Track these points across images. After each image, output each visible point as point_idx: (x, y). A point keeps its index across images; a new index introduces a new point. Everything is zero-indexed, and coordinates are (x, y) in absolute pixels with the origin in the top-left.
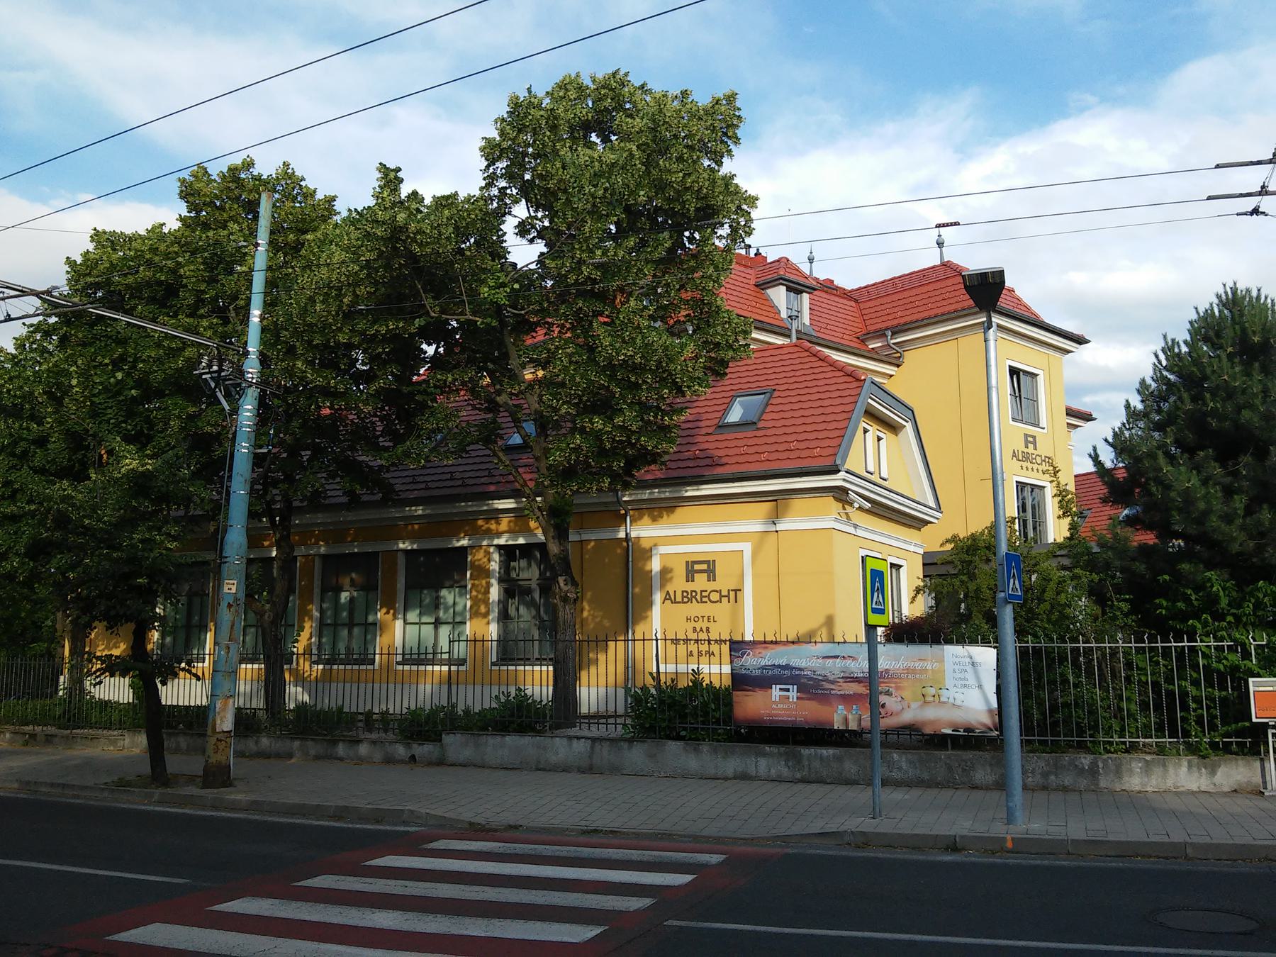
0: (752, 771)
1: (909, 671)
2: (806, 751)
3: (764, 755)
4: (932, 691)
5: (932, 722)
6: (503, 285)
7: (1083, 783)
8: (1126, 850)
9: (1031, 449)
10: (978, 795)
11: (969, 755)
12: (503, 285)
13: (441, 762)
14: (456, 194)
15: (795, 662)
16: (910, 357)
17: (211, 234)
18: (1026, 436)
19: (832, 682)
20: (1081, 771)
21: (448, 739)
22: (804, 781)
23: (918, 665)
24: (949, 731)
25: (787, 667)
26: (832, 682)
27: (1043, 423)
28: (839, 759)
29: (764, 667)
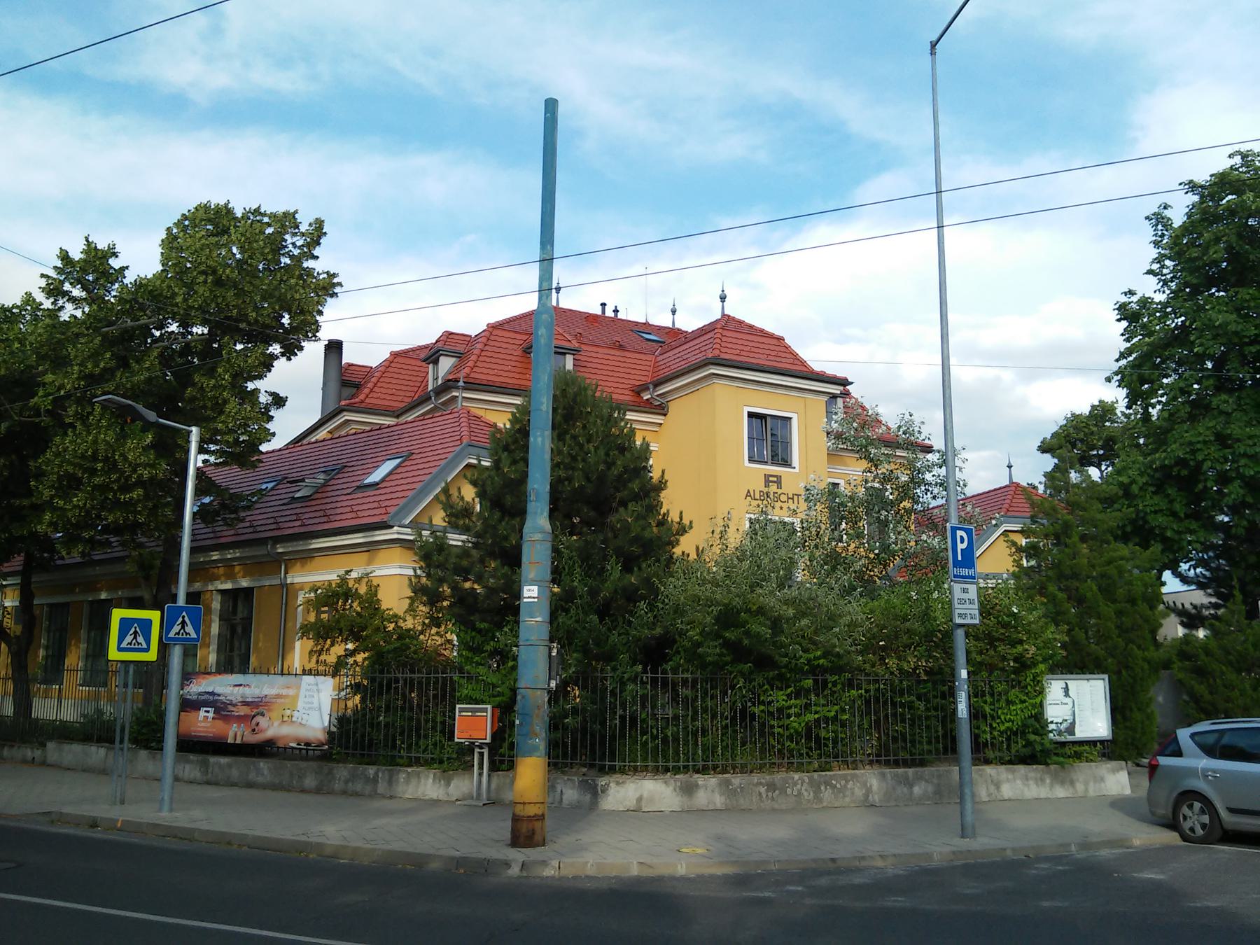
0: (252, 776)
1: (279, 696)
2: (213, 759)
3: (188, 761)
4: (288, 712)
5: (284, 737)
6: (51, 394)
7: (368, 789)
8: (226, 839)
9: (773, 488)
10: (304, 796)
11: (303, 764)
12: (51, 394)
13: (44, 764)
14: (247, 281)
15: (218, 690)
16: (674, 408)
17: (176, 290)
18: (767, 477)
19: (234, 705)
20: (367, 780)
21: (51, 745)
22: (208, 783)
23: (284, 692)
24: (294, 745)
25: (212, 694)
26: (234, 705)
27: (796, 461)
28: (230, 766)
29: (199, 694)
